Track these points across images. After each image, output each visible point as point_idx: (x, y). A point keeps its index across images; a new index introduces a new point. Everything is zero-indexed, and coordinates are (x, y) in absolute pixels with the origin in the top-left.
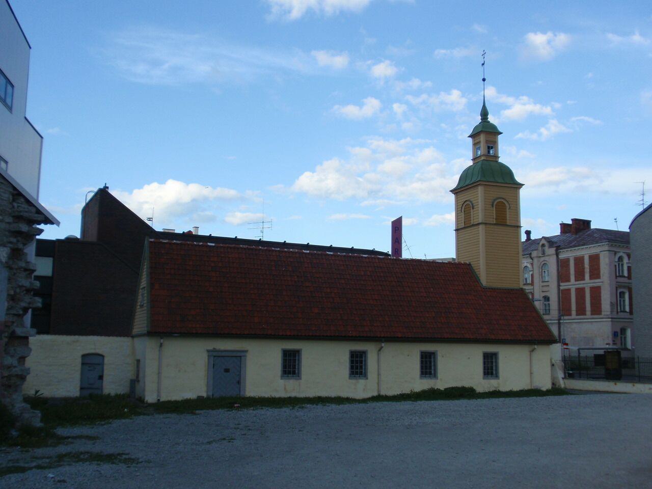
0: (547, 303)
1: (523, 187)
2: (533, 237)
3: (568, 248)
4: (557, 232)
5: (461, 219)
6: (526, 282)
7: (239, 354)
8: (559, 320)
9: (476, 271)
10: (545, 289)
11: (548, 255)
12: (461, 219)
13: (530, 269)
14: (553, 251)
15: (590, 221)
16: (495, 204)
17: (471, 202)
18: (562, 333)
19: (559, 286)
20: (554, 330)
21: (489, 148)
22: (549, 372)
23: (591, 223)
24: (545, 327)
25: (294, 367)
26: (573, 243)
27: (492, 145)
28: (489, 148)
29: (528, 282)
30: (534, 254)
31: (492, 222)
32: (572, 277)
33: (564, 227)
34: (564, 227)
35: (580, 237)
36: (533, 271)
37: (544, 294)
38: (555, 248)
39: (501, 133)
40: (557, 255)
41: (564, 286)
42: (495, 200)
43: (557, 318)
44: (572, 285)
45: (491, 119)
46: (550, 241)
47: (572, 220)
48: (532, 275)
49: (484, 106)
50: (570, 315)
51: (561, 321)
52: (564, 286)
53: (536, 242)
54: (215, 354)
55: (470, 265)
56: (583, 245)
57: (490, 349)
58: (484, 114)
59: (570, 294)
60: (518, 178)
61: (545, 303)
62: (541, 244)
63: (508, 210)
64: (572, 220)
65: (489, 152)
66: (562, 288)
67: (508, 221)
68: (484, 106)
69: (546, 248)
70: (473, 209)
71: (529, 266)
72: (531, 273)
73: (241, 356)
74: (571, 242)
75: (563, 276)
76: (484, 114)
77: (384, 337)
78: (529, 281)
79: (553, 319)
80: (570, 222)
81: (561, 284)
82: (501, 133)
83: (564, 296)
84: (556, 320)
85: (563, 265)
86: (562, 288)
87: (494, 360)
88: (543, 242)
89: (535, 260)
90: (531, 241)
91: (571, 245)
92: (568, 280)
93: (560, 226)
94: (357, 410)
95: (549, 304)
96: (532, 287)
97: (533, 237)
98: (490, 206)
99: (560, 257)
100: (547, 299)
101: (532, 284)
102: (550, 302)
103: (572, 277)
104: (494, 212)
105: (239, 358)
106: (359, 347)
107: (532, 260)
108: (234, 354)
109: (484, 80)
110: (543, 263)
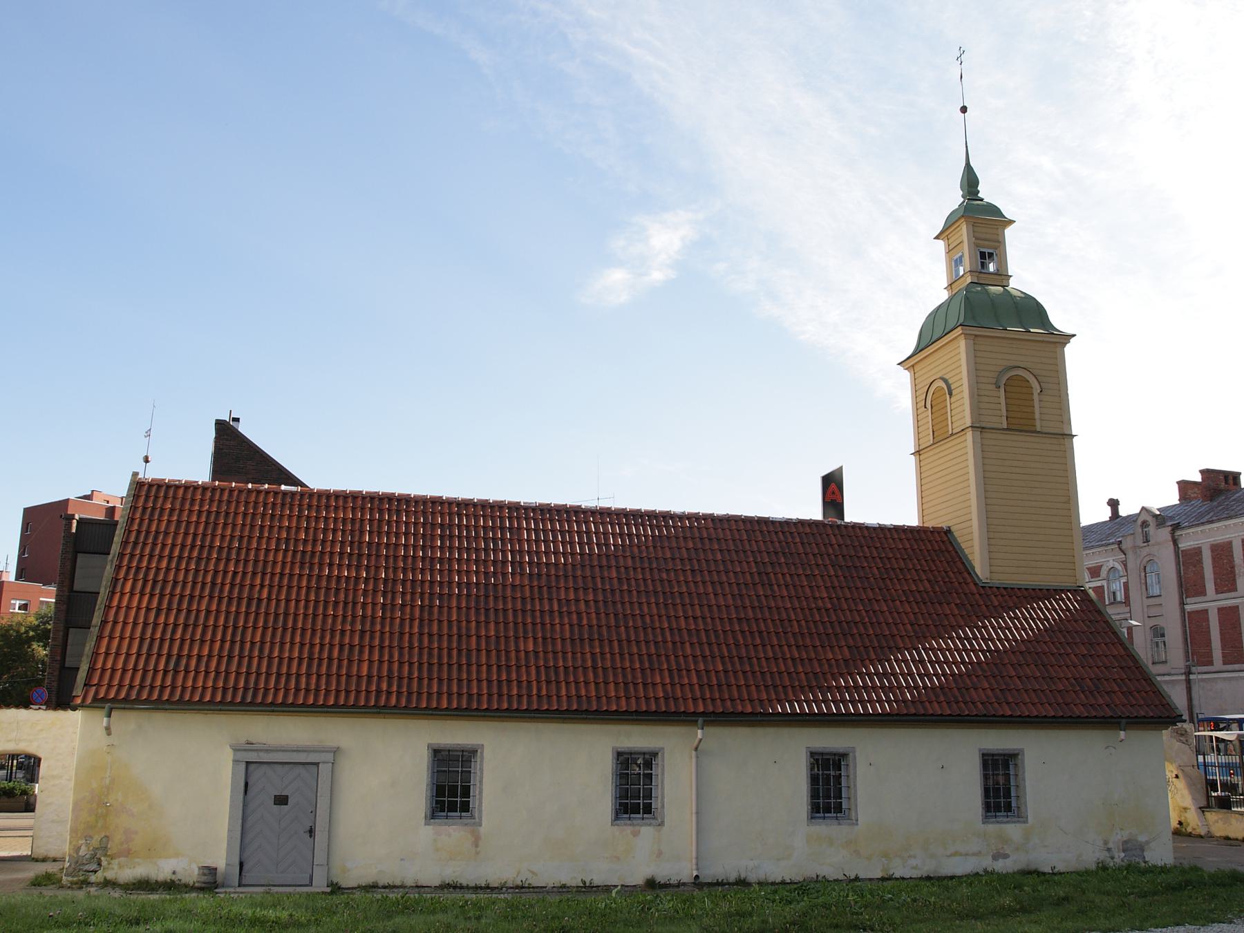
0: (1159, 640)
1: (1072, 340)
2: (1123, 511)
3: (1198, 525)
4: (1172, 498)
5: (925, 421)
6: (1115, 599)
7: (312, 758)
8: (1188, 673)
9: (963, 546)
10: (1153, 612)
11: (1158, 544)
12: (925, 421)
13: (1121, 574)
14: (1165, 533)
15: (1239, 474)
16: (1004, 380)
17: (946, 381)
18: (1195, 702)
19: (1182, 604)
20: (1178, 698)
21: (985, 257)
22: (859, 816)
23: (1241, 476)
24: (1166, 705)
25: (466, 792)
26: (1206, 517)
27: (991, 251)
28: (985, 257)
29: (1119, 599)
30: (1127, 544)
31: (999, 426)
32: (1210, 586)
33: (1184, 486)
34: (1184, 486)
35: (1219, 505)
36: (1127, 576)
37: (1153, 622)
38: (1170, 528)
39: (1012, 222)
40: (1175, 542)
41: (1193, 605)
42: (1001, 373)
43: (1183, 671)
44: (1211, 602)
45: (987, 193)
46: (1162, 518)
47: (1202, 472)
48: (1126, 585)
49: (968, 165)
50: (1210, 663)
51: (1192, 677)
52: (1193, 605)
53: (1132, 519)
54: (253, 757)
55: (948, 532)
56: (1230, 517)
57: (998, 740)
58: (970, 182)
59: (1208, 620)
60: (1059, 320)
61: (1156, 640)
62: (1139, 522)
63: (1036, 397)
64: (1202, 472)
65: (983, 265)
66: (1188, 608)
67: (1038, 423)
68: (968, 165)
69: (1151, 529)
70: (950, 394)
71: (1119, 567)
72: (1124, 580)
73: (317, 764)
74: (1202, 515)
75: (1189, 585)
76: (970, 182)
77: (703, 714)
78: (1120, 596)
79: (1173, 672)
80: (1198, 478)
81: (1189, 600)
82: (1012, 222)
83: (1195, 626)
84: (1182, 674)
85: (1188, 561)
86: (1188, 608)
87: (1012, 772)
88: (1145, 517)
89: (1130, 555)
90: (1119, 519)
91: (1202, 521)
92: (1202, 592)
93: (1177, 486)
94: (818, 892)
95: (1164, 642)
96: (1127, 609)
97: (1123, 511)
98: (993, 387)
99: (1180, 546)
100: (1158, 632)
101: (1127, 602)
102: (1166, 639)
103: (1210, 586)
104: (1003, 401)
105: (314, 768)
106: (637, 738)
107: (1125, 554)
108: (302, 758)
109: (964, 110)
110: (1147, 559)
